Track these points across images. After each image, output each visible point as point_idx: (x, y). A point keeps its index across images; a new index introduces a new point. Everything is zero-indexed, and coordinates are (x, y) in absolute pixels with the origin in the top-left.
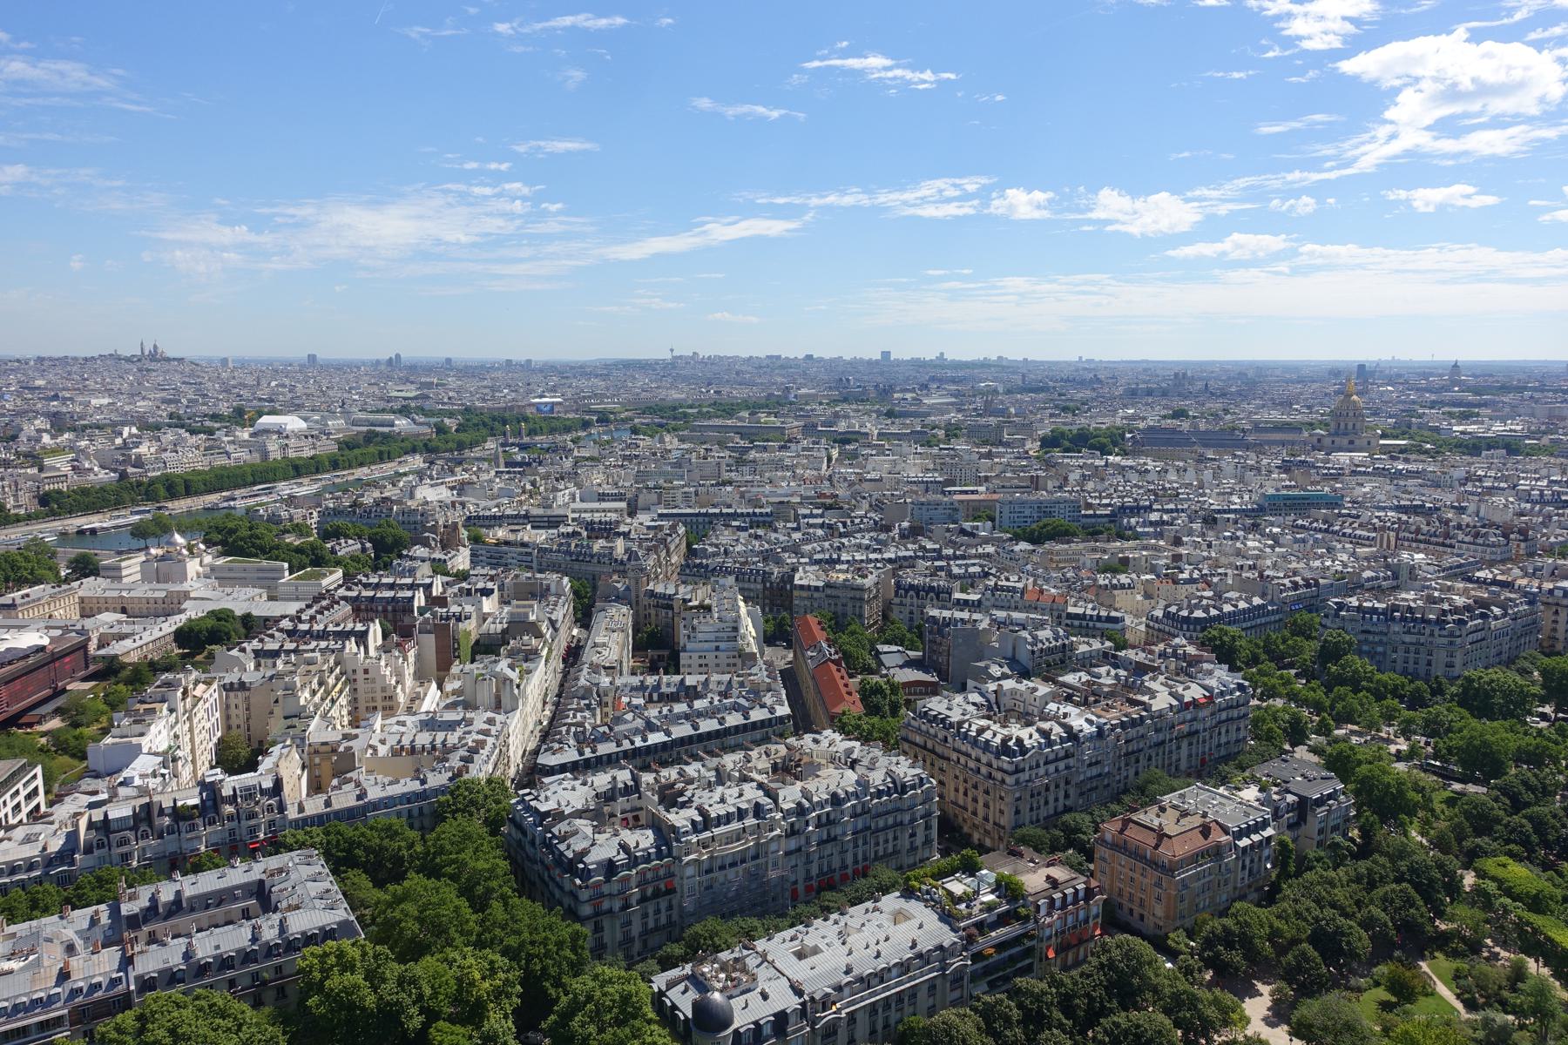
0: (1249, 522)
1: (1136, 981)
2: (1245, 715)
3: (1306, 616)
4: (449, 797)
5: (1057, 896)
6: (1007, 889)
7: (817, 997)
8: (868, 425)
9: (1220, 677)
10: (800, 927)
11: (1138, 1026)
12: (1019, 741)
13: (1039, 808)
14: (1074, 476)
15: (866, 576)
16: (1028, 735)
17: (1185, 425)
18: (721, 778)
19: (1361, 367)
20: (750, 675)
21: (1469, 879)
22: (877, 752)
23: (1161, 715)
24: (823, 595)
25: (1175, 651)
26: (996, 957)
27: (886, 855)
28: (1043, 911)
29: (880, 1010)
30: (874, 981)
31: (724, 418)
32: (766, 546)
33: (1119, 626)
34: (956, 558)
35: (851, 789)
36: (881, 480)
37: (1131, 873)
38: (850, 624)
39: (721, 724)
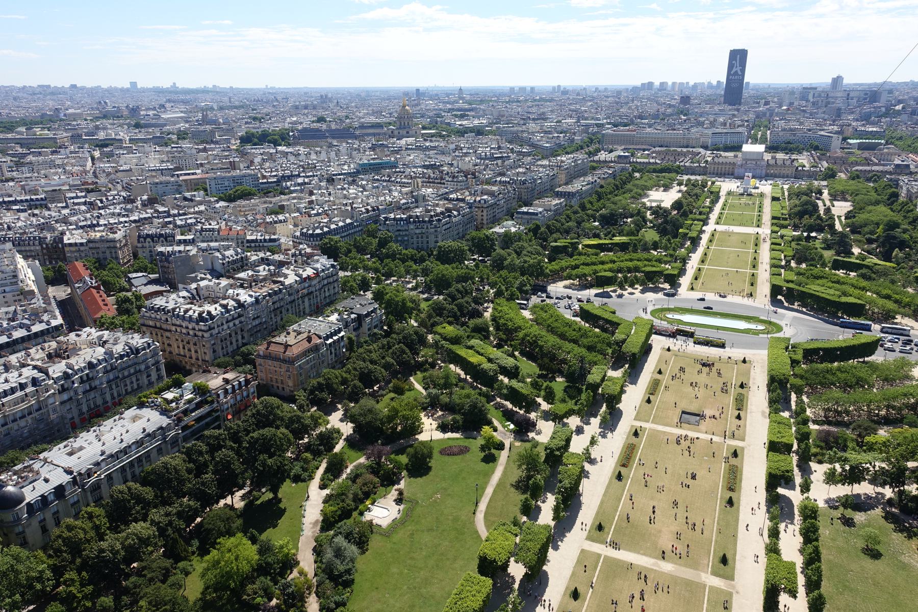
0: (350, 179)
3: (374, 226)
5: (229, 387)
6: (200, 390)
8: (122, 134)
9: (323, 262)
11: (263, 435)
12: (209, 313)
13: (227, 347)
14: (257, 160)
15: (116, 233)
16: (214, 309)
17: (324, 127)
19: (418, 90)
20: (30, 304)
21: (430, 337)
23: (291, 286)
24: (87, 248)
25: (300, 252)
26: (197, 426)
29: (128, 469)
31: (6, 133)
32: (42, 221)
33: (277, 243)
34: (180, 215)
35: (101, 358)
36: (130, 170)
37: (275, 369)
38: (109, 264)
39: (9, 338)
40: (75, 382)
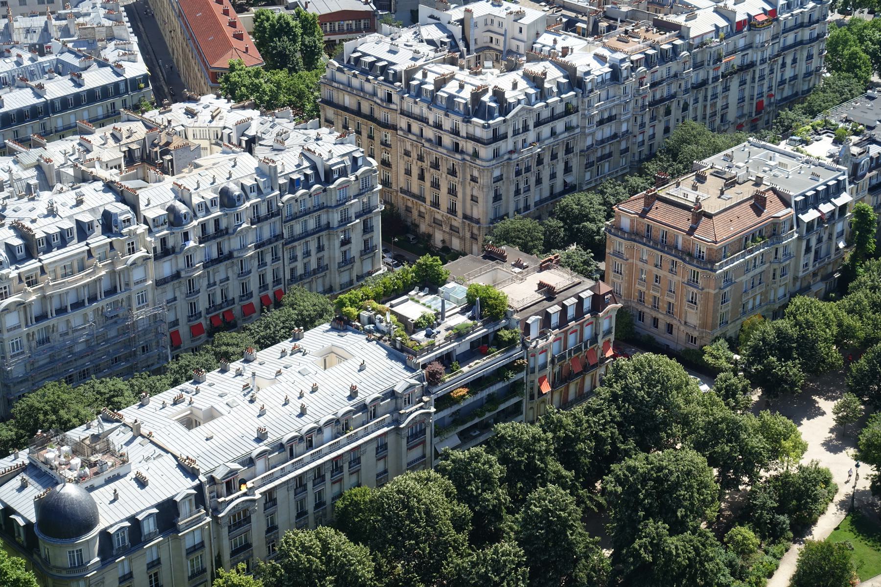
1: (660, 412)
2: (820, 36)
5: (554, 309)
7: (218, 475)
10: (187, 385)
11: (660, 469)
12: (498, 95)
13: (527, 190)
20: (78, 15)
26: (470, 399)
28: (534, 332)
29: (310, 485)
30: (299, 448)
35: (249, 182)
37: (656, 271)
40: (191, 236)
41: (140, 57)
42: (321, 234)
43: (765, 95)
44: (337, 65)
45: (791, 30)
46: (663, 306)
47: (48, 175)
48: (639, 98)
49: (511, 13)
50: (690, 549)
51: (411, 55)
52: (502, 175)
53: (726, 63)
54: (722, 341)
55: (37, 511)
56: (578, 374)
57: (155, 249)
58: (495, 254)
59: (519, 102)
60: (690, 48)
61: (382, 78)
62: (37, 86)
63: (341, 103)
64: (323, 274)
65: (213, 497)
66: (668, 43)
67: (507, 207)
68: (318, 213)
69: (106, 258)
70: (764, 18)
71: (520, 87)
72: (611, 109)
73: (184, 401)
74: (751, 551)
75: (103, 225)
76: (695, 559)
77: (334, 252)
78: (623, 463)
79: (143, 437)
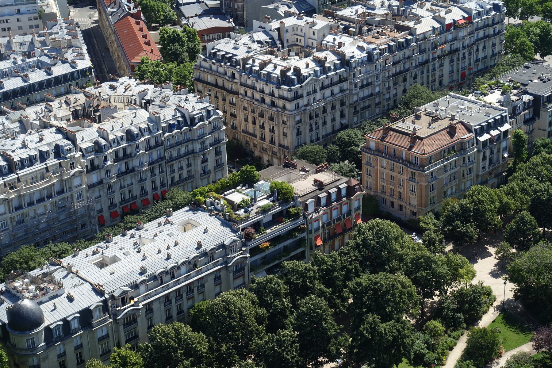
1: (384, 254)
2: (500, 32)
4: (242, 364)
5: (323, 195)
7: (116, 294)
10: (102, 244)
11: (376, 283)
12: (297, 71)
13: (318, 128)
18: (24, 126)
20: (51, 34)
22: (168, 92)
23: (425, 37)
26: (272, 249)
27: (181, 180)
28: (311, 209)
29: (173, 301)
30: (166, 278)
35: (143, 126)
37: (391, 173)
39: (25, 81)
40: (109, 158)
41: (87, 57)
42: (189, 156)
43: (467, 68)
44: (203, 57)
45: (481, 28)
46: (396, 194)
47: (26, 125)
48: (386, 72)
49: (308, 23)
50: (395, 331)
51: (246, 49)
52: (301, 120)
53: (441, 49)
54: (430, 214)
55: (8, 315)
56: (340, 234)
57: (87, 166)
58: (290, 164)
59: (310, 75)
60: (417, 41)
61: (229, 64)
62: (24, 76)
63: (206, 80)
64: (191, 180)
65: (114, 307)
66: (403, 38)
67: (305, 139)
68: (187, 144)
69: (57, 172)
70: (463, 21)
71: (310, 66)
72: (368, 78)
73: (99, 252)
74: (440, 335)
75: (55, 153)
76: (398, 336)
77: (198, 167)
78: (354, 281)
79: (73, 273)
